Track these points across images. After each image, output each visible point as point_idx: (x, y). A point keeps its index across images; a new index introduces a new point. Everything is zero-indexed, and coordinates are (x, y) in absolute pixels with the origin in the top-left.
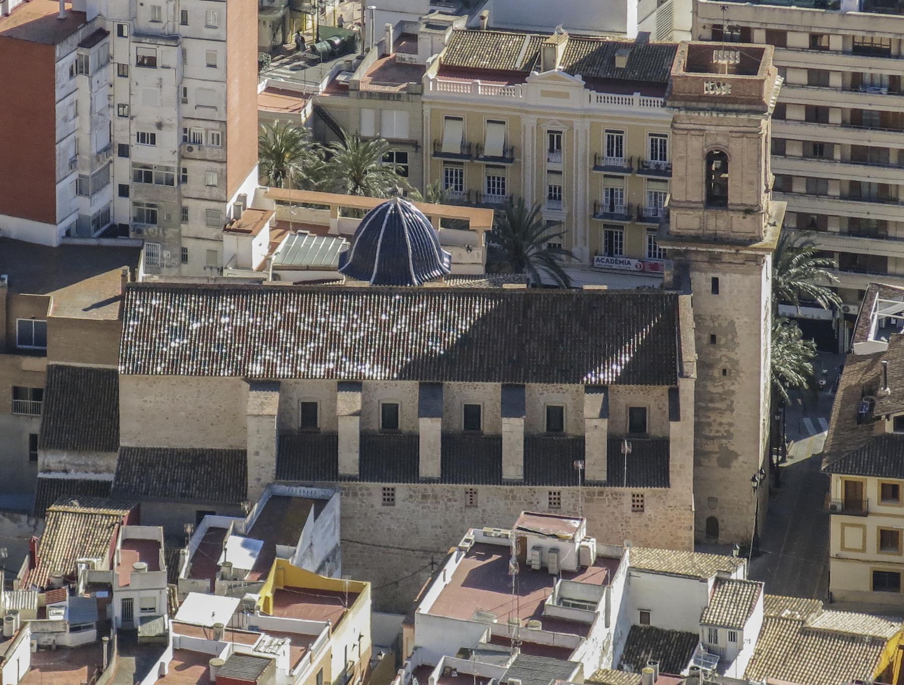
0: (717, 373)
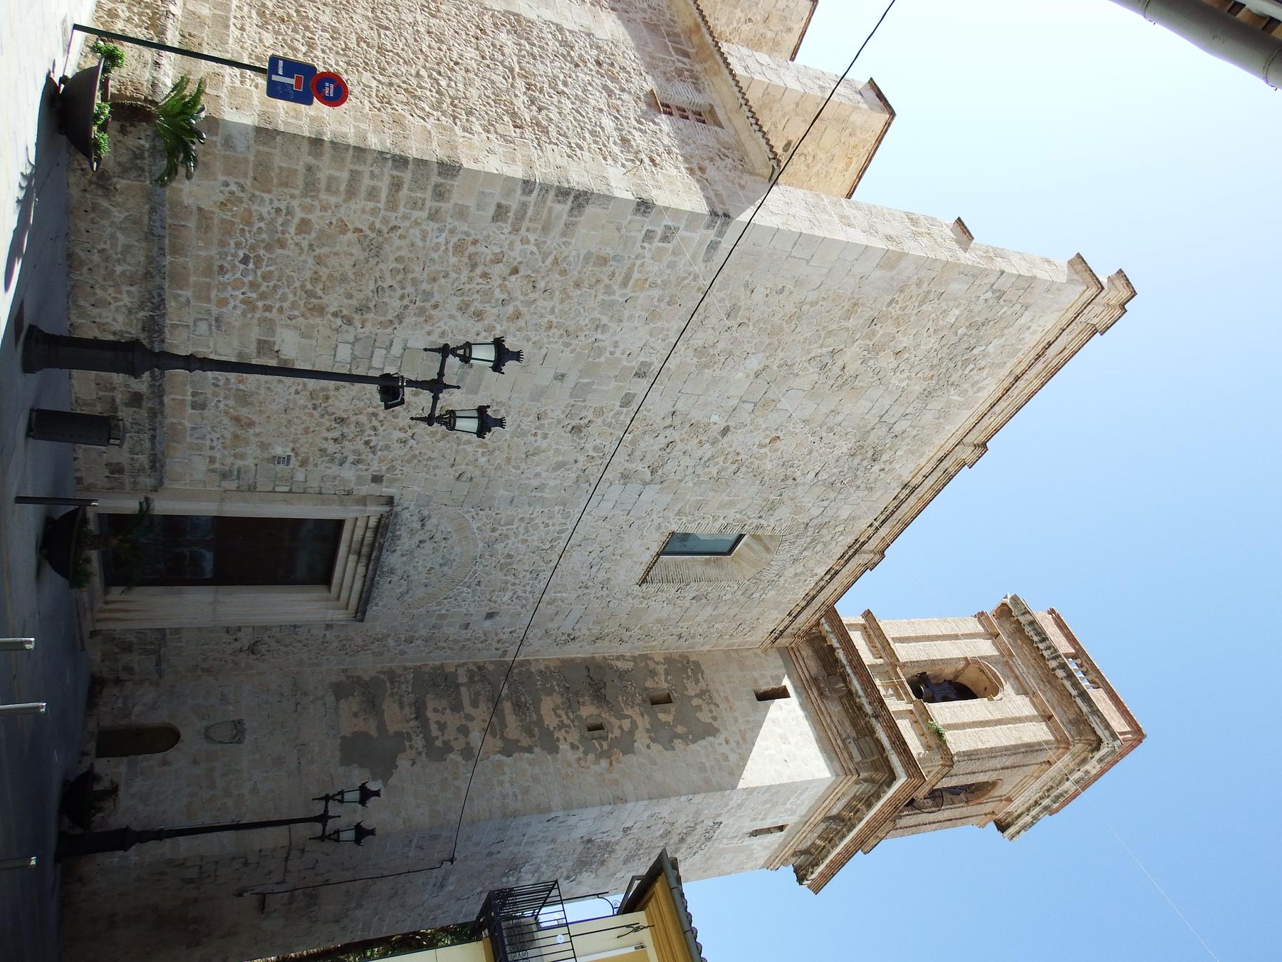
0: (588, 711)
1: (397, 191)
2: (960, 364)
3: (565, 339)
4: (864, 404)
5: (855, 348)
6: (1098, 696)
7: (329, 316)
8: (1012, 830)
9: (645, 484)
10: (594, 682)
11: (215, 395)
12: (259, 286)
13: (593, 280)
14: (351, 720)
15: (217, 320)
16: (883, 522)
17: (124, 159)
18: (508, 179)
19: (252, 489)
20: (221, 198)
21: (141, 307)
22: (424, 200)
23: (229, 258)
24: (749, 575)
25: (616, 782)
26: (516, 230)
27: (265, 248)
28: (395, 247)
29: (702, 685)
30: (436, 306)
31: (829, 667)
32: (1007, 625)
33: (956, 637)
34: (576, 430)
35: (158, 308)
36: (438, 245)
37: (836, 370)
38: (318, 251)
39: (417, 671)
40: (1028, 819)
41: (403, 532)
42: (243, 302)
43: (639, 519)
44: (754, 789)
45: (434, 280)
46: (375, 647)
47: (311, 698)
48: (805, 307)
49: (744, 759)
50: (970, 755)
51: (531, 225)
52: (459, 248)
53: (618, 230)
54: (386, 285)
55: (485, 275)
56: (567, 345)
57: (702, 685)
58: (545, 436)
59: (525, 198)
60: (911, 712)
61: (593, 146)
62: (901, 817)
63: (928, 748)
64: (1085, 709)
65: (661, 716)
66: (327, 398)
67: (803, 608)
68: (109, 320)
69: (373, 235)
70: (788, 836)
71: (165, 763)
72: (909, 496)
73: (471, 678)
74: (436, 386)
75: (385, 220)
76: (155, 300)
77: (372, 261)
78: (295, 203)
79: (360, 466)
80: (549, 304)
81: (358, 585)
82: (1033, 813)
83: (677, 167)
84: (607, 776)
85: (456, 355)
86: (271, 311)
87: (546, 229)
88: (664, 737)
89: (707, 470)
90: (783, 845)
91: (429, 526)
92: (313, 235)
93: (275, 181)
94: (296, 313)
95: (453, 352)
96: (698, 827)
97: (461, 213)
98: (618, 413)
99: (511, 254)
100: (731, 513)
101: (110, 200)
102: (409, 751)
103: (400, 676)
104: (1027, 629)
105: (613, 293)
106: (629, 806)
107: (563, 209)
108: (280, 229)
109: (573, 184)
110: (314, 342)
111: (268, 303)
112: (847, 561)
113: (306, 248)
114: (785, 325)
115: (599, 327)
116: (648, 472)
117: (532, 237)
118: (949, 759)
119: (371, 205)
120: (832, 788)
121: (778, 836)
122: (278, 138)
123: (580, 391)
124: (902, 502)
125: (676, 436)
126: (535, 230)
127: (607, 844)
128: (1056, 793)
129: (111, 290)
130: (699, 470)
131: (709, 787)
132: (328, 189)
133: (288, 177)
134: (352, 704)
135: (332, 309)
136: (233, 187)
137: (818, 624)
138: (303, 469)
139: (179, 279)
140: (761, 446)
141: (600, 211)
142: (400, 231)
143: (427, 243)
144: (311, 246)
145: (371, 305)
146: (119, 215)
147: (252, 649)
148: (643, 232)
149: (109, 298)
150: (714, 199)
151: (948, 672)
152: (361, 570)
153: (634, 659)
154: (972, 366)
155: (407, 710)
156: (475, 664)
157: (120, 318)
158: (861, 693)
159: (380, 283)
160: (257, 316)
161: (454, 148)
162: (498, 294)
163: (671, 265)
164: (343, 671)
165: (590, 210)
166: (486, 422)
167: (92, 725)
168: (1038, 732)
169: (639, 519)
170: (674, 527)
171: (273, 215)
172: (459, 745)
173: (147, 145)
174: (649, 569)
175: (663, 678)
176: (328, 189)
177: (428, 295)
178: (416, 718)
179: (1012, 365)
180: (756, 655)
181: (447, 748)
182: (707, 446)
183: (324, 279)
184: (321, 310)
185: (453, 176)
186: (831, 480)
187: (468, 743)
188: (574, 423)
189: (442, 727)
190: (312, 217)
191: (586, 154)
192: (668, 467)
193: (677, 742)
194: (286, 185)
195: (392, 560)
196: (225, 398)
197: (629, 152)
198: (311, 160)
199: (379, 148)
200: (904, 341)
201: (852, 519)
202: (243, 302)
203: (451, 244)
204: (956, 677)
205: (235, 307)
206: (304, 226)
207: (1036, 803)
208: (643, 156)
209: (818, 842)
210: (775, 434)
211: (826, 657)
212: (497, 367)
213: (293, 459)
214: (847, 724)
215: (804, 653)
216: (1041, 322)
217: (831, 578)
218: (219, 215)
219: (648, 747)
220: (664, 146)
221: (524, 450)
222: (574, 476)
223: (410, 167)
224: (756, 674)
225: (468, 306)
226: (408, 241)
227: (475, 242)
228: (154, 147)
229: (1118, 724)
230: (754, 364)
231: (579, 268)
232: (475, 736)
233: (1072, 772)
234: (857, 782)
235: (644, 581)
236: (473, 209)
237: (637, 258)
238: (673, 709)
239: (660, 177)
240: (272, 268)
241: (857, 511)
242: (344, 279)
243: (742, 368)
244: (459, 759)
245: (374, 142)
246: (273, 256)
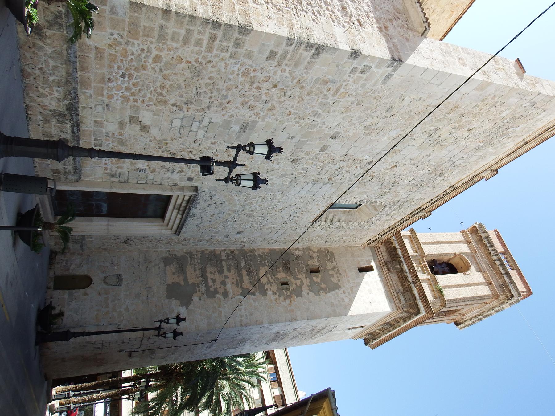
1: (213, 41)
4: (445, 152)
5: (449, 128)
6: (513, 273)
7: (169, 105)
9: (324, 184)
10: (284, 260)
11: (107, 140)
12: (131, 89)
13: (318, 92)
14: (172, 276)
15: (107, 105)
16: (436, 201)
17: (50, 18)
18: (279, 37)
19: (126, 182)
20: (109, 42)
21: (65, 98)
22: (228, 47)
23: (114, 74)
24: (364, 219)
25: (293, 311)
26: (279, 65)
27: (135, 70)
28: (209, 72)
29: (334, 264)
30: (229, 102)
31: (393, 257)
32: (475, 237)
33: (451, 242)
35: (74, 99)
36: (233, 72)
37: (435, 137)
38: (165, 72)
39: (203, 252)
41: (201, 201)
42: (121, 97)
43: (317, 198)
44: (355, 316)
45: (230, 89)
46: (184, 243)
47: (153, 264)
49: (351, 301)
50: (453, 301)
51: (289, 63)
52: (245, 73)
53: (338, 66)
54: (202, 91)
55: (258, 88)
56: (297, 123)
57: (334, 264)
58: (278, 163)
59: (288, 48)
60: (428, 279)
61: (326, 12)
63: (435, 297)
64: (507, 280)
65: (315, 279)
66: (166, 144)
68: (48, 104)
69: (197, 65)
71: (85, 294)
73: (228, 257)
74: (232, 164)
75: (204, 58)
76: (73, 95)
77: (195, 79)
78: (153, 46)
79: (182, 174)
80: (291, 103)
81: (177, 222)
82: (473, 320)
83: (372, 27)
84: (289, 308)
85: (244, 150)
86: (137, 102)
87: (296, 65)
88: (316, 289)
91: (214, 198)
92: (163, 64)
93: (141, 33)
94: (151, 103)
95: (244, 148)
97: (249, 55)
98: (318, 154)
99: (275, 77)
101: (43, 41)
102: (198, 292)
103: (195, 255)
104: (485, 240)
105: (328, 99)
107: (308, 55)
108: (143, 60)
109: (316, 40)
110: (161, 118)
111: (136, 98)
113: (158, 71)
114: (416, 116)
115: (317, 115)
116: (327, 179)
117: (287, 69)
118: (444, 303)
119: (197, 49)
120: (390, 315)
122: (143, 8)
123: (300, 144)
124: (448, 193)
125: (345, 164)
126: (290, 65)
127: (285, 334)
129: (47, 89)
131: (335, 314)
132: (172, 39)
133: (149, 31)
134: (172, 268)
135: (171, 102)
136: (116, 36)
138: (152, 174)
139: (85, 84)
140: (386, 169)
141: (329, 56)
142: (212, 64)
143: (228, 70)
144: (161, 70)
145: (193, 101)
146: (49, 50)
147: (126, 242)
148: (351, 68)
149: (47, 94)
150: (393, 49)
151: (445, 259)
152: (179, 216)
153: (303, 250)
154: (505, 136)
155: (197, 272)
156: (230, 250)
157: (54, 103)
158: (407, 271)
159: (199, 90)
160: (130, 104)
161: (248, 16)
162: (264, 97)
163: (363, 86)
164: (168, 251)
165: (324, 55)
166: (258, 181)
167: (52, 274)
168: (485, 291)
169: (317, 198)
171: (140, 52)
172: (221, 290)
173: (64, 11)
176: (172, 39)
177: (225, 97)
178: (202, 276)
179: (526, 137)
180: (360, 249)
181: (216, 292)
182: (359, 169)
183: (167, 86)
184: (165, 103)
185: (247, 35)
187: (225, 290)
188: (294, 158)
189: (214, 281)
190: (163, 54)
191: (323, 18)
193: (321, 292)
194: (148, 36)
195: (194, 211)
196: (112, 142)
197: (346, 16)
198: (163, 22)
199: (204, 16)
200: (475, 124)
201: (421, 199)
202: (121, 97)
203: (241, 71)
204: (449, 260)
205: (117, 99)
206: (157, 59)
207: (475, 317)
208: (354, 19)
211: (392, 252)
212: (268, 157)
213: (147, 170)
215: (382, 249)
216: (549, 118)
217: (403, 222)
218: (108, 51)
219: (308, 294)
220: (366, 12)
221: (267, 169)
222: (290, 180)
223: (222, 28)
224: (359, 259)
225: (247, 103)
226: (217, 69)
227: (255, 71)
228: (68, 12)
229: (521, 288)
231: (311, 85)
232: (229, 287)
233: (496, 306)
236: (256, 53)
237: (344, 81)
238: (320, 276)
239: (363, 34)
240: (138, 80)
241: (424, 197)
242: (179, 87)
243: (387, 135)
244: (221, 297)
245: (202, 12)
246: (139, 74)
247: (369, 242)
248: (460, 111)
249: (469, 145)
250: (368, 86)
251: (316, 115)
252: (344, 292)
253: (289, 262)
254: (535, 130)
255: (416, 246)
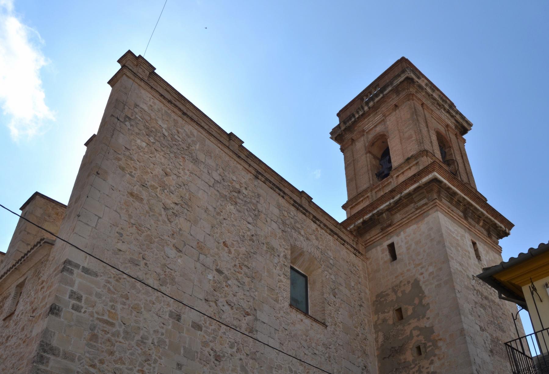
0: (409, 356)
2: (174, 142)
3: (151, 362)
8: (465, 125)
9: (256, 319)
13: (108, 343)
34: (218, 358)
40: (458, 117)
43: (281, 325)
48: (132, 221)
56: (155, 361)
62: (463, 181)
65: (409, 313)
67: (339, 236)
70: (479, 240)
72: (262, 175)
82: (454, 114)
89: (246, 283)
90: (485, 243)
96: (476, 288)
100: (276, 272)
104: (348, 124)
106: (465, 326)
112: (307, 211)
116: (248, 318)
121: (480, 246)
127: (492, 341)
128: (440, 101)
130: (247, 288)
137: (351, 232)
140: (230, 252)
148: (73, 311)
153: (377, 332)
158: (388, 203)
163: (99, 295)
165: (55, 343)
170: (287, 304)
174: (315, 320)
175: (386, 314)
180: (370, 264)
182: (229, 282)
186: (253, 216)
188: (214, 360)
192: (245, 306)
193: (424, 302)
200: (158, 170)
201: (279, 207)
207: (448, 112)
209: (481, 224)
210: (222, 244)
214: (407, 209)
215: (368, 238)
216: (148, 99)
217: (319, 220)
219: (428, 318)
222: (251, 361)
230: (172, 253)
233: (427, 93)
234: (441, 201)
235: (324, 324)
247: (357, 254)
248: (136, 189)
249: (189, 170)
250: (99, 290)
251: (142, 342)
252: (422, 274)
253: (392, 348)
254: (166, 109)
255: (362, 199)
